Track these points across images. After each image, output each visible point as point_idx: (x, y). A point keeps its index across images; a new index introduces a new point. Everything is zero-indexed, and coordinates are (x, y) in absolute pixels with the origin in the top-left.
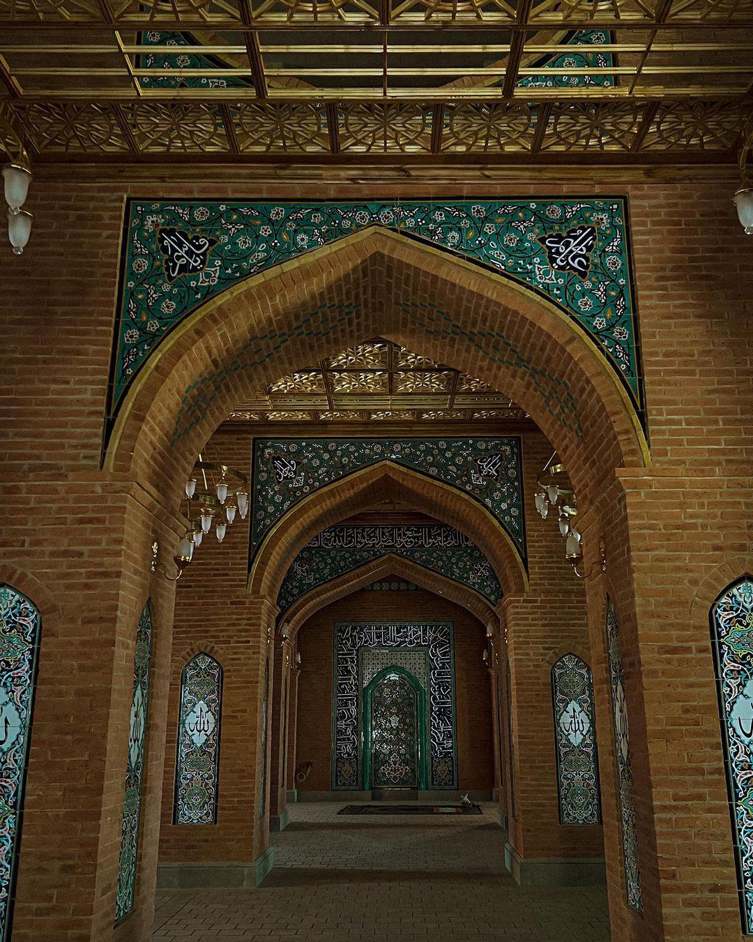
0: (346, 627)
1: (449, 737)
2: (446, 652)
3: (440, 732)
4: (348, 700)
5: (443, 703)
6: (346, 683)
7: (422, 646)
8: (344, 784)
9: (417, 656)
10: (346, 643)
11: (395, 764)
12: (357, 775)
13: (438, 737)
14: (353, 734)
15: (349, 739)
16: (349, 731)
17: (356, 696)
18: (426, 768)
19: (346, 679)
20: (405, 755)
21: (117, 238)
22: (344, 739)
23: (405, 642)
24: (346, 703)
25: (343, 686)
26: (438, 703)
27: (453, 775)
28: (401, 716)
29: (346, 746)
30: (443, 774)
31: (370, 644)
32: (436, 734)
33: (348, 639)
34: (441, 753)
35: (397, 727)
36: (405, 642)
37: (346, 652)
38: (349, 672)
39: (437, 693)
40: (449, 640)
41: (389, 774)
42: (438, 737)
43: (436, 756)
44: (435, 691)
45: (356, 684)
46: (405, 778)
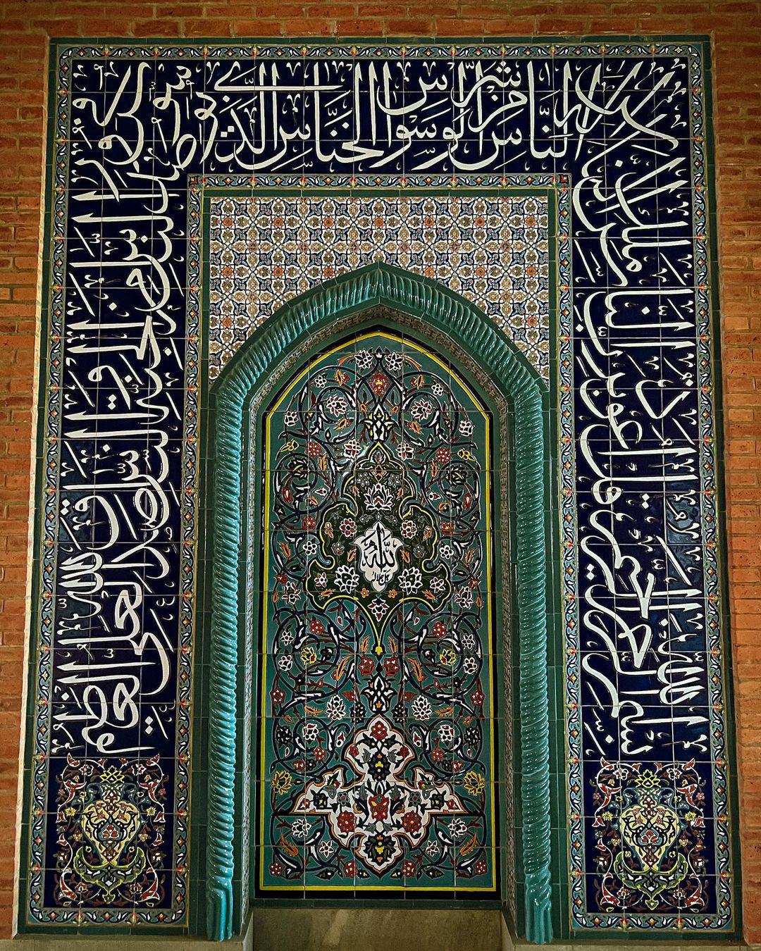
0: (121, 67)
1: (689, 647)
2: (667, 199)
3: (633, 619)
4: (118, 445)
5: (647, 466)
6: (111, 358)
7: (536, 165)
8: (93, 899)
9: (504, 221)
10: (117, 152)
11: (379, 775)
12: (167, 848)
13: (623, 645)
14: (148, 625)
15: (125, 653)
16: (128, 606)
17: (170, 424)
18: (558, 818)
19: (110, 337)
20: (432, 726)
21: (43, 56)
22: (99, 654)
23: (442, 146)
24: (113, 460)
25: (95, 374)
26: (620, 466)
27: (708, 854)
28: (409, 529)
29: (109, 688)
30: (651, 849)
31: (247, 156)
32: (613, 629)
33: (127, 129)
34: (638, 736)
35: (394, 584)
36: (442, 146)
37: (116, 195)
38: (132, 303)
39: (613, 412)
40: (681, 133)
41: (347, 822)
42: (623, 645)
43: (612, 752)
44: (602, 402)
45: (168, 365)
46: (432, 849)
